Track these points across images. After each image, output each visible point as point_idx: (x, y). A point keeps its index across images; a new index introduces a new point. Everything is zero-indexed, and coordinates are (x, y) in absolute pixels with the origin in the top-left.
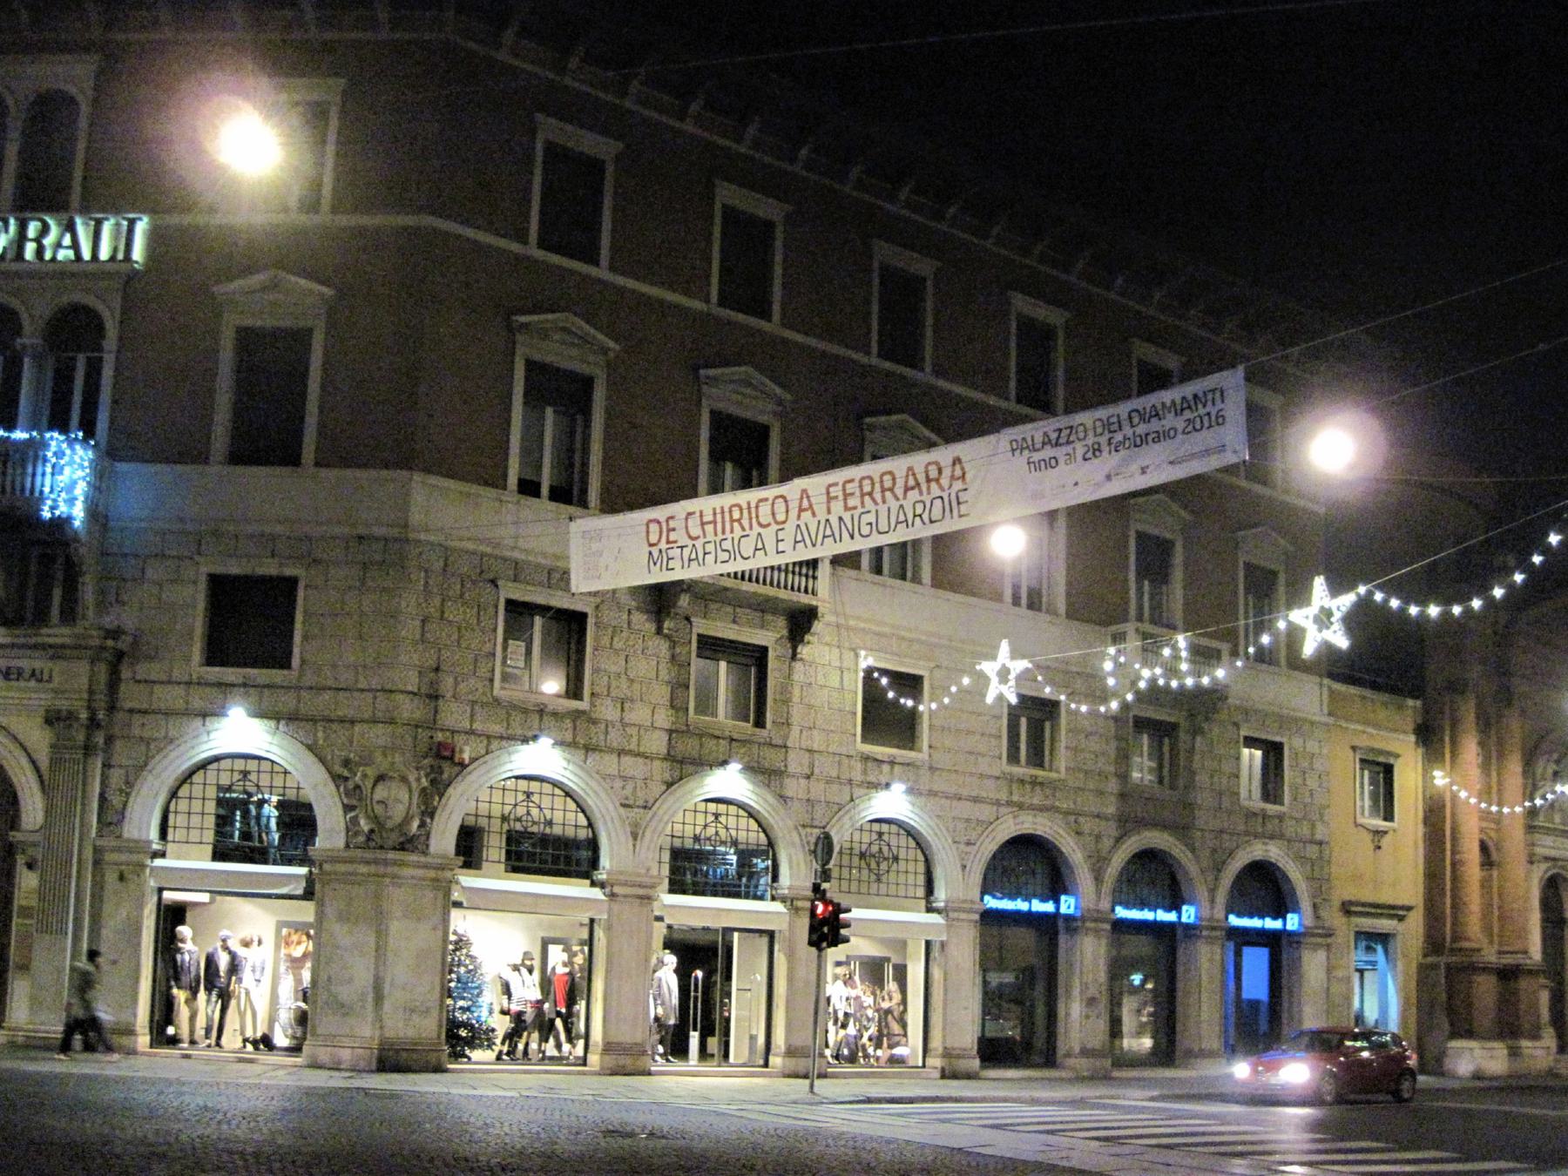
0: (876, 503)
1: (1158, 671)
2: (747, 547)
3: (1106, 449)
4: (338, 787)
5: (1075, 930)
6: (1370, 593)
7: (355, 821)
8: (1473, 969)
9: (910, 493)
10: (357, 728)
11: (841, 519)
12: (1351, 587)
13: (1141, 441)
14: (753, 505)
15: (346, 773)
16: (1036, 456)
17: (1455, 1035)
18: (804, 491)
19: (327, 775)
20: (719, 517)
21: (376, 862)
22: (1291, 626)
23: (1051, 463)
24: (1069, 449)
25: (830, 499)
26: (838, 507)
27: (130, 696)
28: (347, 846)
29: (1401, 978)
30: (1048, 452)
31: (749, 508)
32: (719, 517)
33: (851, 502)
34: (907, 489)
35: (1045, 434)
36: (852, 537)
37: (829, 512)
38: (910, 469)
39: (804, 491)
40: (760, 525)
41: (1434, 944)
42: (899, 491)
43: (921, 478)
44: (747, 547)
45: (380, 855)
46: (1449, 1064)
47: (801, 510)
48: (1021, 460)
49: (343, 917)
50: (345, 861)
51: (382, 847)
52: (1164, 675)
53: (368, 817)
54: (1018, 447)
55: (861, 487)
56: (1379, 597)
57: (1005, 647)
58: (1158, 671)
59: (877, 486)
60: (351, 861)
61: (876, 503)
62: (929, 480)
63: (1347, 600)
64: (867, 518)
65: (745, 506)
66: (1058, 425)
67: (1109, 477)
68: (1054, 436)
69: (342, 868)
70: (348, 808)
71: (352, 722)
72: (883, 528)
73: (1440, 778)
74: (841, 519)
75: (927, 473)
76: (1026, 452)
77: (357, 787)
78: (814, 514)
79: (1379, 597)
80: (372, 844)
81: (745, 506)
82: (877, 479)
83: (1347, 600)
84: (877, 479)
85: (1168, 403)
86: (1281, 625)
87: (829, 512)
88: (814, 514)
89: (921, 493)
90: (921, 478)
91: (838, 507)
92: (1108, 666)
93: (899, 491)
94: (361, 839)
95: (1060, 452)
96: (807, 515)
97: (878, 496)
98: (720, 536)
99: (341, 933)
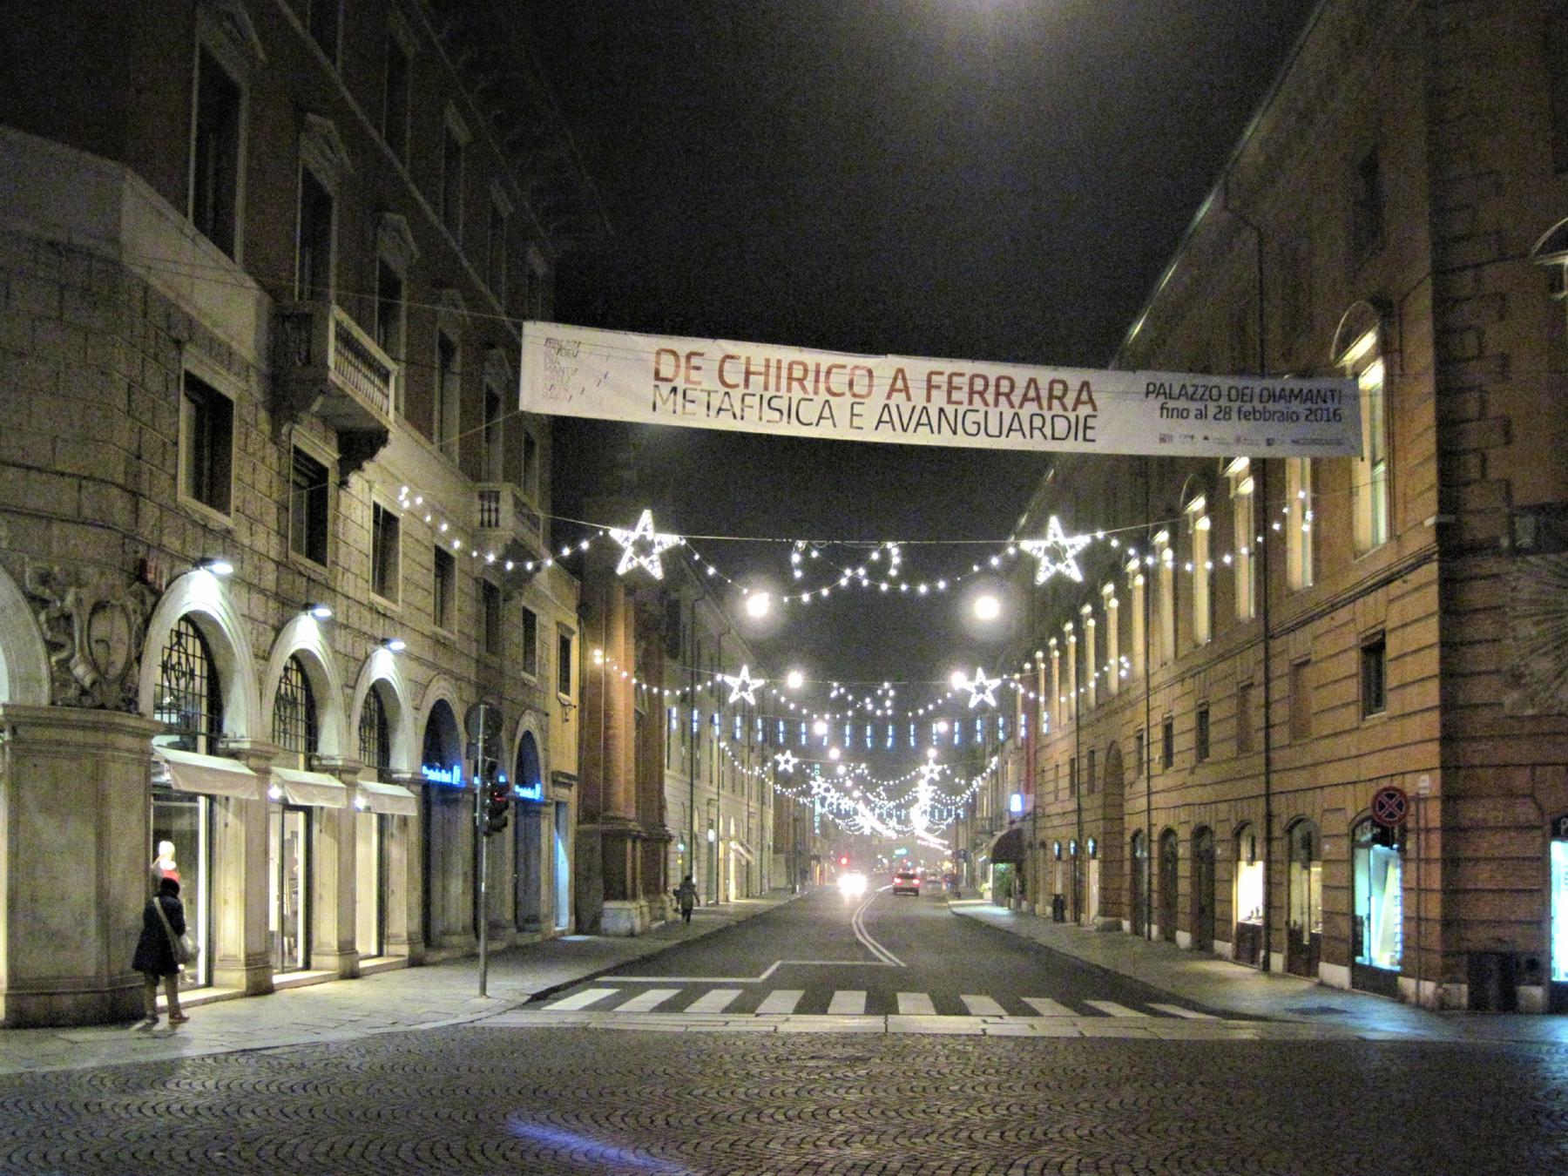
0: (986, 404)
1: (861, 571)
2: (809, 412)
3: (1235, 415)
4: (36, 614)
5: (456, 801)
6: (1107, 540)
7: (64, 665)
8: (622, 835)
9: (1027, 404)
10: (56, 530)
11: (941, 410)
12: (1089, 528)
13: (1266, 416)
14: (823, 369)
15: (47, 594)
16: (1171, 404)
17: (607, 898)
18: (901, 371)
19: (20, 596)
20: (773, 371)
21: (95, 727)
22: (1021, 555)
23: (1182, 414)
24: (1200, 405)
25: (930, 387)
26: (939, 398)
28: (53, 703)
29: (571, 840)
30: (1181, 404)
31: (818, 373)
32: (773, 371)
33: (956, 396)
34: (1025, 399)
35: (1184, 386)
36: (955, 432)
37: (929, 400)
38: (1032, 381)
39: (901, 371)
40: (829, 390)
41: (588, 814)
42: (1016, 399)
43: (1044, 394)
44: (809, 412)
45: (103, 716)
46: (606, 923)
47: (893, 389)
48: (1154, 403)
49: (47, 809)
50: (49, 724)
51: (102, 706)
52: (869, 575)
53: (85, 660)
54: (1152, 391)
55: (971, 384)
56: (1115, 543)
57: (647, 517)
58: (861, 571)
59: (992, 389)
60: (68, 725)
61: (986, 404)
62: (1051, 397)
63: (1082, 541)
64: (971, 417)
65: (812, 367)
66: (1195, 381)
67: (1238, 440)
68: (1190, 390)
69: (49, 734)
70: (53, 647)
71: (50, 520)
72: (993, 430)
73: (598, 657)
74: (941, 410)
75: (1051, 390)
76: (1161, 398)
77: (68, 618)
78: (909, 399)
79: (1115, 543)
80: (88, 701)
81: (812, 367)
82: (992, 382)
83: (1082, 541)
84: (992, 382)
85: (1296, 391)
86: (1011, 551)
87: (929, 400)
88: (909, 399)
89: (1041, 407)
90: (1044, 394)
91: (939, 398)
92: (796, 558)
93: (1016, 399)
94: (72, 692)
95: (1194, 407)
96: (898, 398)
97: (990, 397)
98: (771, 392)
99: (47, 830)
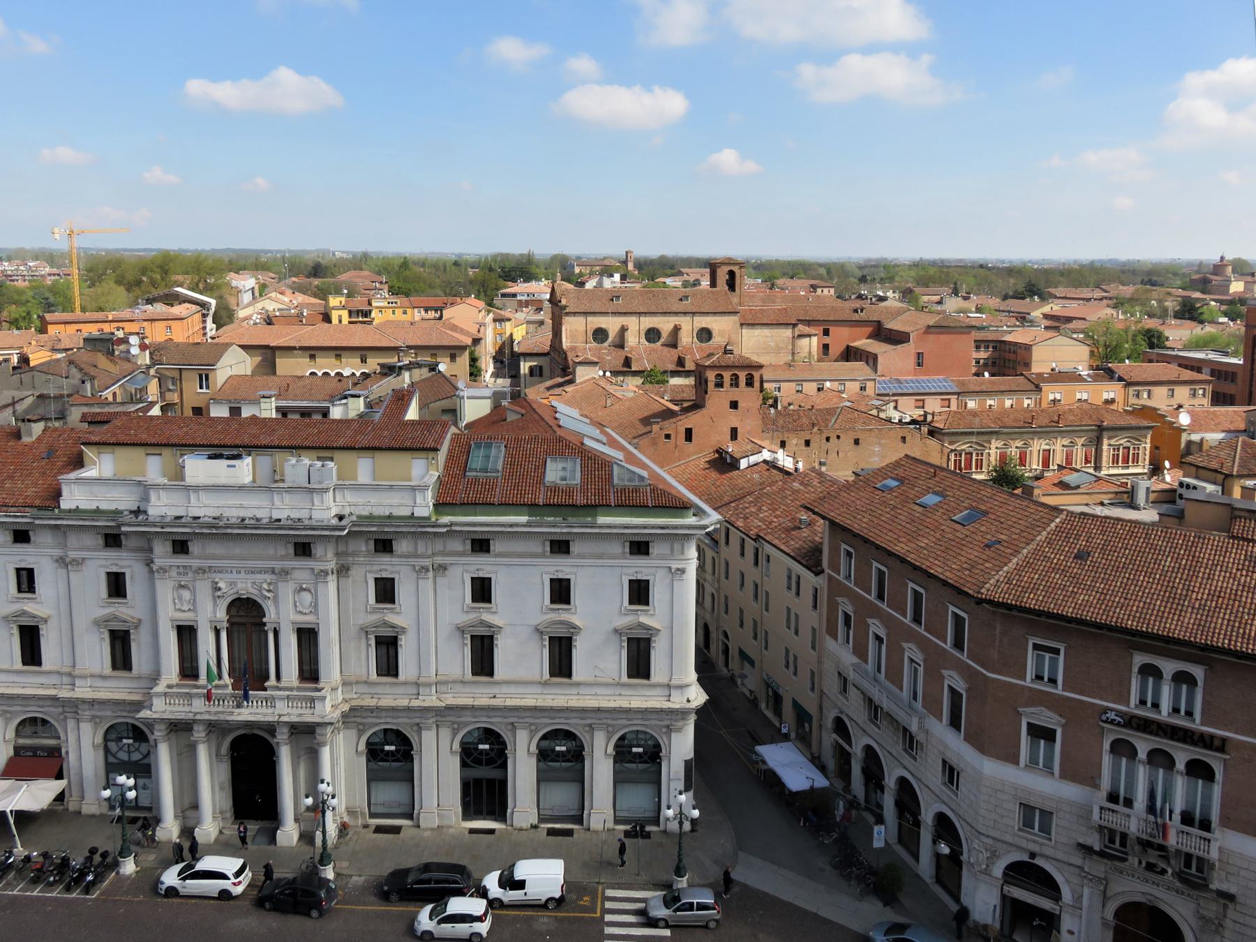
27: (1230, 913)
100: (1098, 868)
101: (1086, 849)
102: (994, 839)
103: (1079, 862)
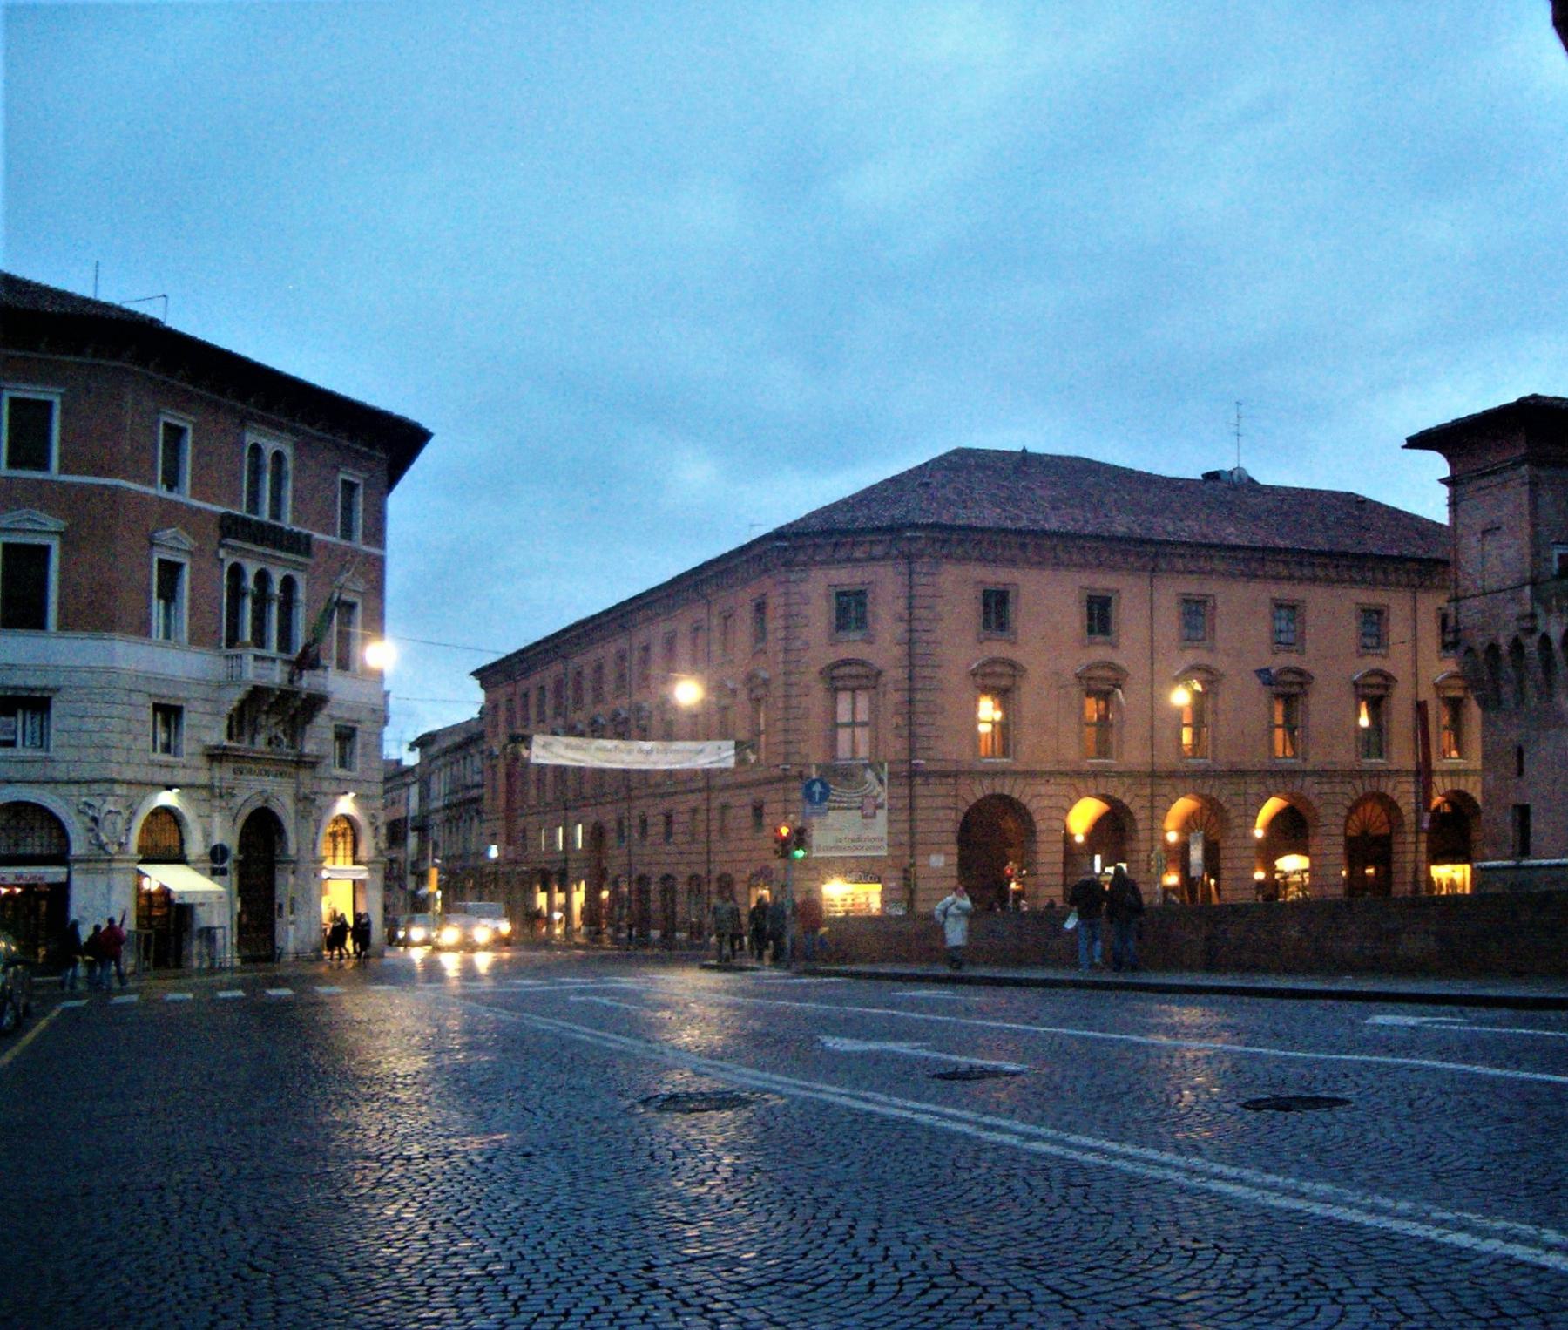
100: (224, 774)
101: (216, 756)
102: (130, 783)
103: (203, 778)
